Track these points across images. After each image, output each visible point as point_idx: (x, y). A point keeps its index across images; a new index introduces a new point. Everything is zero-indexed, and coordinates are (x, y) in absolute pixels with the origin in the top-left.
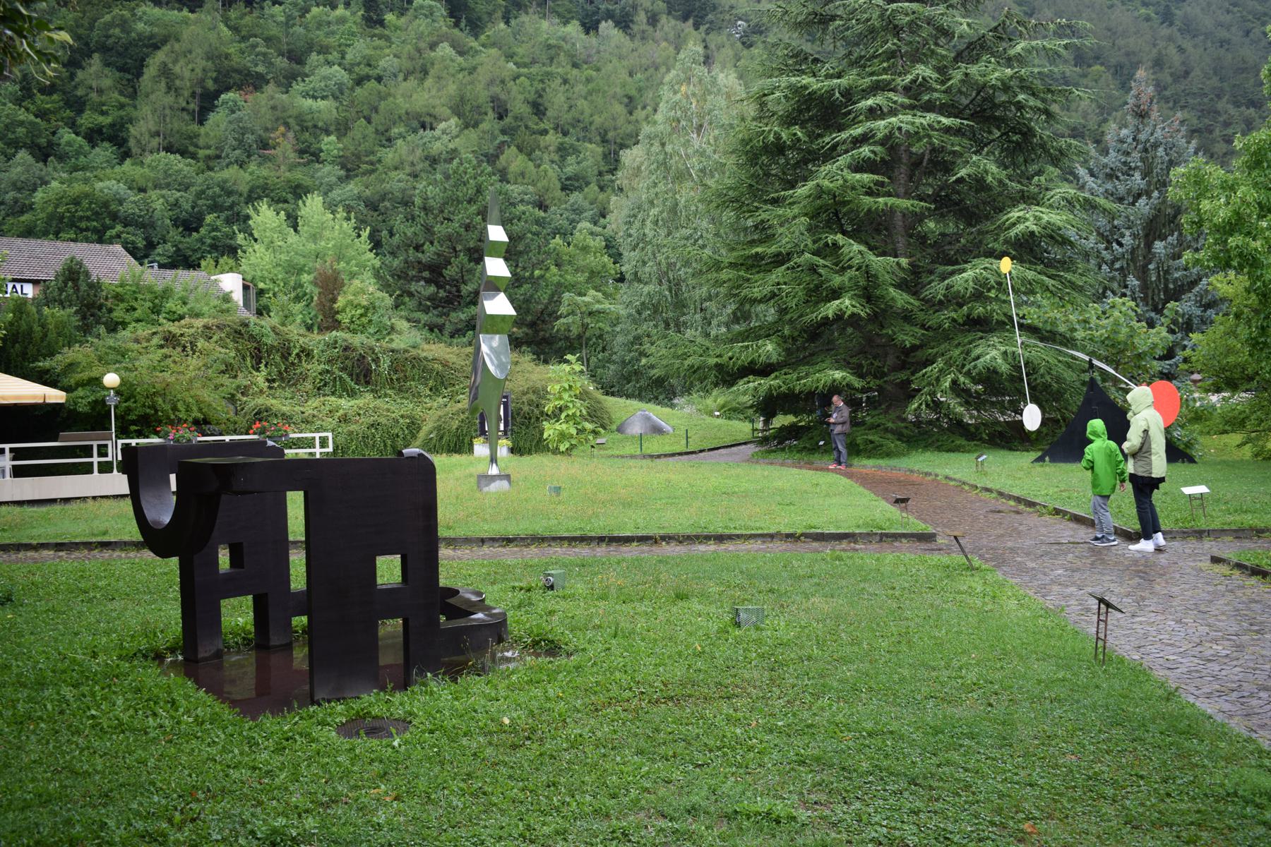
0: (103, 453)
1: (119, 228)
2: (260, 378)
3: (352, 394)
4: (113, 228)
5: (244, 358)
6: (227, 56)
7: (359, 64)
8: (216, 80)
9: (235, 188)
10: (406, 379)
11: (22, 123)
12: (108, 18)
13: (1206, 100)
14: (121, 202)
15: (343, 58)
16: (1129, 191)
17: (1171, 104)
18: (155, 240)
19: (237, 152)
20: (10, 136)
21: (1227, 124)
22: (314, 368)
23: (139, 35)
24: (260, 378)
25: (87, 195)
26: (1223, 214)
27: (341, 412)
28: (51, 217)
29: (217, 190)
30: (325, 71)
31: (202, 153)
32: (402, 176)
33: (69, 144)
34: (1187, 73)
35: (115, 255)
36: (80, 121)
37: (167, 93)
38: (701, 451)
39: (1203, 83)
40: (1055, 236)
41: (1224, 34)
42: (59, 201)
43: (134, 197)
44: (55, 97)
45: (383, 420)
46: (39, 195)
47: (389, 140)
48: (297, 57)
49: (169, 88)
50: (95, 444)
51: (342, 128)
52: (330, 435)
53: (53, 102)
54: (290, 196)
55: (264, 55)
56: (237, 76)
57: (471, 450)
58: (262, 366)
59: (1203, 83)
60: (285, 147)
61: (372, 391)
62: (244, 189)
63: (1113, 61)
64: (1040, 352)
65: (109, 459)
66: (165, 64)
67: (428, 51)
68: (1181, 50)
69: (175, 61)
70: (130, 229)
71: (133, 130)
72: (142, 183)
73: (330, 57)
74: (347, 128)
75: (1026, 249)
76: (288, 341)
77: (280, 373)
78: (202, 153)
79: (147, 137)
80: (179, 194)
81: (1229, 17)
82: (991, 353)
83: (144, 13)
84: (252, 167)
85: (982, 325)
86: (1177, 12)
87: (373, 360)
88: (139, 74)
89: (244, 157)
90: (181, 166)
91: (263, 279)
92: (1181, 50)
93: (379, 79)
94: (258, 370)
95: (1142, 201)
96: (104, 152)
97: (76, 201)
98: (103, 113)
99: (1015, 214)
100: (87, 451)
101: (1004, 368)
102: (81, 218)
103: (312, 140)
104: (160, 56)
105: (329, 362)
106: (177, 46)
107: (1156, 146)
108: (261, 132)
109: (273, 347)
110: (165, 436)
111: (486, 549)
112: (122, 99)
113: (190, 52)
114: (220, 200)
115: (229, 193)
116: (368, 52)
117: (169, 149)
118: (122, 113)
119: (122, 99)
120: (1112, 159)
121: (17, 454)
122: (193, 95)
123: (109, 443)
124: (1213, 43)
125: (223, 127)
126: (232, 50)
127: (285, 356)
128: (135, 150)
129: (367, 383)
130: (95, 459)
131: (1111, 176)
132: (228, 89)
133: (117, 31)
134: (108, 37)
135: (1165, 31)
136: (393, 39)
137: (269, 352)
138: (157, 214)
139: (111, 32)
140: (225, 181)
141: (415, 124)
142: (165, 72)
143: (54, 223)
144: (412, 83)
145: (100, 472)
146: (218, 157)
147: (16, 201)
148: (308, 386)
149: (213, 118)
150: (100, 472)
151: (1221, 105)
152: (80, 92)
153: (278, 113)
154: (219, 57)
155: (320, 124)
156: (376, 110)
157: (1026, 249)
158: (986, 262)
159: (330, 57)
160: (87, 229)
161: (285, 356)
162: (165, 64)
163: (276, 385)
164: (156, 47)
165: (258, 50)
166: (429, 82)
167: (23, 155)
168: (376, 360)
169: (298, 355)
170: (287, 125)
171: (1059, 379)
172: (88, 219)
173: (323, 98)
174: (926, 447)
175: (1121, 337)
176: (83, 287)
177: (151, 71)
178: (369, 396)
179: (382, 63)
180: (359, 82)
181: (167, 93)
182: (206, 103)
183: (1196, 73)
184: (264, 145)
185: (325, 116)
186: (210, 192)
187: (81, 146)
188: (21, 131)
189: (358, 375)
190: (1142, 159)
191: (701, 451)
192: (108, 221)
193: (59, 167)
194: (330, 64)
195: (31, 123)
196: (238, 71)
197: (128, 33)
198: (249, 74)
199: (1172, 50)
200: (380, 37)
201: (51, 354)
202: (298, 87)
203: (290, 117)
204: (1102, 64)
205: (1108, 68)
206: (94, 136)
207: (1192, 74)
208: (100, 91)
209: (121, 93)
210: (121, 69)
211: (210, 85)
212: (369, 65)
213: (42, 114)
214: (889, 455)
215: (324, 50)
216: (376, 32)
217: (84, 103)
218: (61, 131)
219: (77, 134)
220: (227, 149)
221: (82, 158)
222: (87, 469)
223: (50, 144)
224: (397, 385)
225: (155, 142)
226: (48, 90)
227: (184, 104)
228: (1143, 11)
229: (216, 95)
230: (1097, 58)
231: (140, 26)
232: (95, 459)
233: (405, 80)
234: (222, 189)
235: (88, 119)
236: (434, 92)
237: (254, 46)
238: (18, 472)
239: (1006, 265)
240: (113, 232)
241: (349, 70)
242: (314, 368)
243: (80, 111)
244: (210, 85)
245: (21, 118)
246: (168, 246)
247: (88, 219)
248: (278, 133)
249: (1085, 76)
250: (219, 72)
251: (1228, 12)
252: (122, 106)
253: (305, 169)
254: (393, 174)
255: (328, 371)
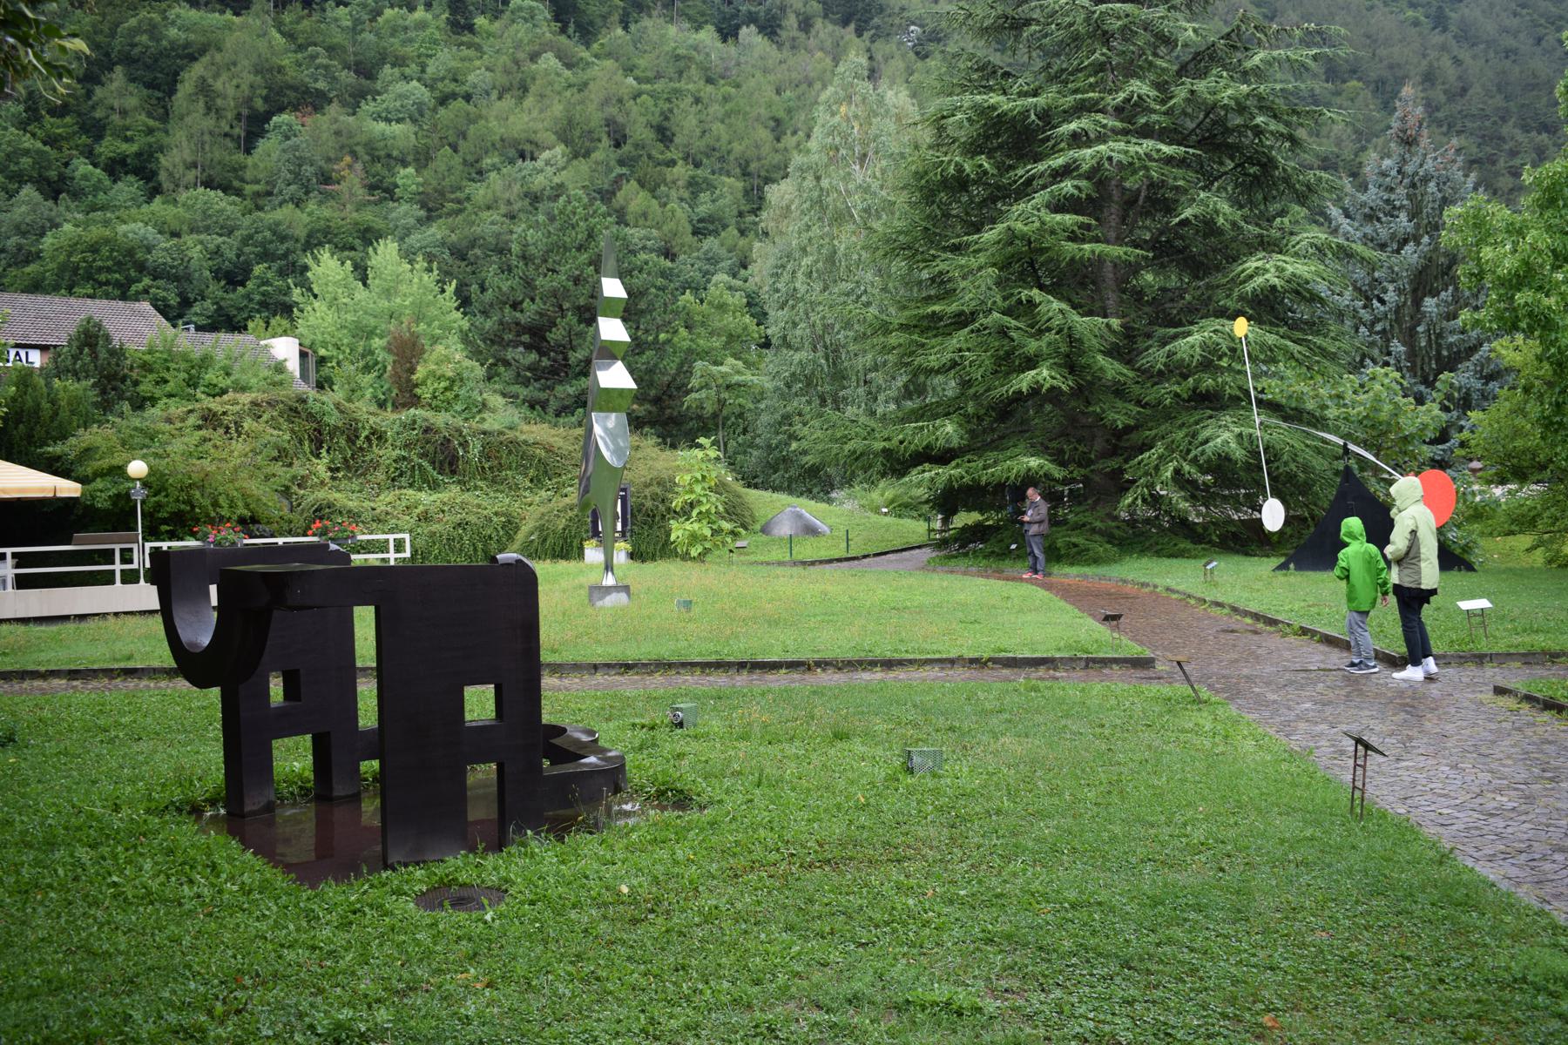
0: (128, 559)
1: (147, 281)
2: (321, 467)
3: (434, 486)
4: (139, 281)
5: (301, 442)
6: (280, 69)
7: (443, 79)
8: (266, 99)
9: (290, 232)
10: (501, 467)
11: (27, 152)
12: (133, 22)
13: (1487, 123)
14: (149, 249)
15: (423, 71)
16: (1393, 236)
17: (1444, 129)
18: (192, 296)
19: (293, 187)
20: (13, 167)
21: (1513, 153)
22: (387, 454)
23: (172, 43)
24: (321, 467)
25: (107, 241)
26: (1509, 264)
27: (421, 508)
28: (63, 268)
29: (268, 234)
30: (401, 87)
31: (249, 189)
32: (496, 217)
33: (85, 177)
34: (1464, 90)
35: (142, 315)
36: (98, 149)
37: (206, 115)
38: (865, 557)
39: (1485, 103)
40: (1302, 291)
41: (1509, 42)
42: (73, 248)
43: (165, 243)
44: (68, 119)
45: (472, 519)
46: (48, 241)
47: (480, 173)
48: (366, 70)
49: (208, 109)
50: (117, 547)
51: (422, 158)
52: (407, 536)
53: (65, 126)
54: (357, 242)
55: (326, 67)
56: (292, 94)
57: (581, 555)
58: (323, 452)
59: (1485, 103)
60: (352, 181)
61: (459, 482)
62: (301, 233)
63: (1373, 75)
64: (1283, 434)
65: (135, 566)
66: (203, 79)
67: (528, 63)
68: (1457, 61)
69: (216, 76)
70: (161, 282)
71: (164, 161)
72: (175, 226)
73: (407, 71)
74: (428, 158)
75: (1266, 307)
76: (356, 420)
77: (345, 460)
78: (249, 189)
79: (181, 169)
80: (220, 240)
81: (1516, 21)
82: (1223, 435)
83: (178, 16)
84: (311, 206)
85: (1211, 401)
86: (1452, 15)
87: (460, 444)
88: (172, 92)
89: (301, 194)
90: (223, 204)
91: (325, 345)
92: (1457, 61)
93: (468, 98)
94: (318, 456)
95: (1409, 248)
96: (128, 188)
97: (94, 248)
98: (127, 140)
99: (1252, 264)
100: (108, 557)
101: (1238, 453)
102: (100, 269)
103: (385, 172)
104: (198, 69)
105: (406, 446)
106: (218, 57)
107: (1426, 180)
108: (322, 163)
109: (336, 428)
110: (204, 538)
111: (599, 678)
112: (151, 122)
113: (235, 64)
114: (272, 246)
115: (283, 238)
116: (454, 64)
117: (209, 184)
118: (151, 139)
119: (151, 122)
120: (1372, 196)
121: (21, 561)
122: (238, 117)
123: (135, 547)
124: (1496, 53)
125: (275, 156)
126: (286, 62)
127: (352, 439)
128: (166, 185)
129: (453, 472)
130: (118, 567)
131: (1370, 217)
132: (281, 110)
133: (144, 38)
134: (133, 45)
135: (1437, 38)
136: (485, 48)
137: (332, 435)
138: (194, 264)
139: (137, 39)
140: (278, 224)
141: (512, 153)
142: (204, 88)
143: (67, 275)
144: (508, 102)
145: (124, 582)
146: (269, 194)
147: (20, 248)
148: (380, 476)
149: (262, 145)
150: (124, 582)
151: (1506, 130)
152: (98, 114)
153: (343, 140)
154: (270, 70)
155: (395, 153)
156: (464, 135)
157: (1266, 307)
158: (1216, 324)
159: (407, 71)
160: (107, 283)
161: (352, 439)
162: (203, 79)
163: (340, 475)
164: (193, 58)
165: (318, 61)
166: (529, 101)
167: (28, 192)
168: (464, 445)
169: (367, 438)
170: (354, 154)
171: (1306, 468)
172: (109, 270)
173: (399, 121)
174: (1143, 552)
175: (1384, 416)
176: (103, 354)
177: (186, 87)
178: (456, 489)
179: (471, 78)
180: (443, 101)
181: (206, 115)
182: (254, 127)
183: (1476, 90)
184: (326, 179)
185: (401, 144)
186: (259, 237)
187: (100, 181)
188: (26, 161)
189: (441, 463)
190: (1409, 197)
191: (865, 557)
192: (133, 273)
193: (73, 206)
194: (407, 78)
195: (39, 152)
196: (294, 88)
197: (158, 41)
198: (307, 91)
199: (1446, 62)
200: (469, 46)
201: (64, 437)
202: (368, 107)
203: (358, 144)
204: (1359, 79)
205: (1367, 83)
206: (116, 168)
207: (1471, 92)
208: (124, 113)
209: (150, 115)
210: (149, 86)
211: (259, 104)
212: (456, 81)
213: (52, 141)
214: (1096, 561)
215: (399, 62)
216: (464, 39)
217: (104, 128)
218: (75, 161)
219: (95, 165)
220: (280, 184)
221: (101, 195)
222: (107, 579)
223: (62, 178)
224: (489, 475)
225: (191, 176)
226: (59, 111)
227: (227, 129)
228: (1410, 13)
229: (267, 117)
230: (1354, 71)
231: (173, 32)
232: (118, 567)
233: (500, 98)
234: (274, 233)
235: (109, 147)
236: (535, 113)
237: (313, 57)
238: (22, 583)
239: (1241, 327)
240: (140, 286)
241: (430, 87)
242: (387, 454)
243: (99, 138)
244: (259, 104)
245: (27, 145)
246: (208, 304)
247: (109, 270)
248: (343, 164)
249: (1338, 93)
250: (270, 88)
251: (1515, 15)
252: (150, 131)
253: (376, 209)
254: (485, 215)
255: (404, 458)
